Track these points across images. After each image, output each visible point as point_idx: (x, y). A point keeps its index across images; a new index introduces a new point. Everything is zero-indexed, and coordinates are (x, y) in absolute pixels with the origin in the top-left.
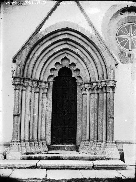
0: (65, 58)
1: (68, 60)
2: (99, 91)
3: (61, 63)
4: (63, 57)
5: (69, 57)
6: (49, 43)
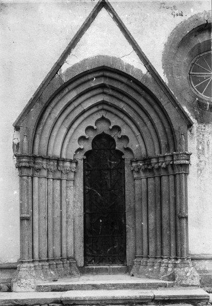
1: (109, 122)
2: (163, 173)
3: (95, 127)
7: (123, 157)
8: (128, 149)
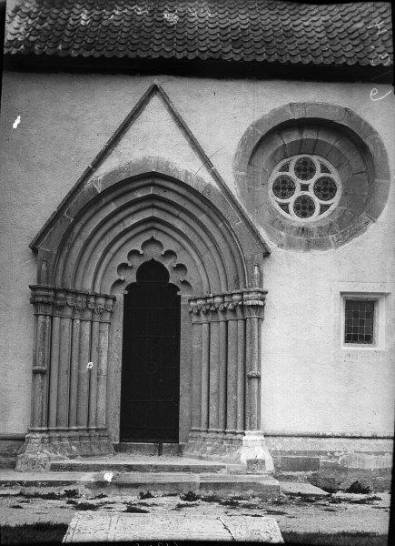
0: (152, 241)
1: (159, 244)
2: (229, 316)
3: (141, 252)
4: (146, 237)
5: (159, 237)
6: (113, 207)
7: (178, 293)
8: (185, 283)
